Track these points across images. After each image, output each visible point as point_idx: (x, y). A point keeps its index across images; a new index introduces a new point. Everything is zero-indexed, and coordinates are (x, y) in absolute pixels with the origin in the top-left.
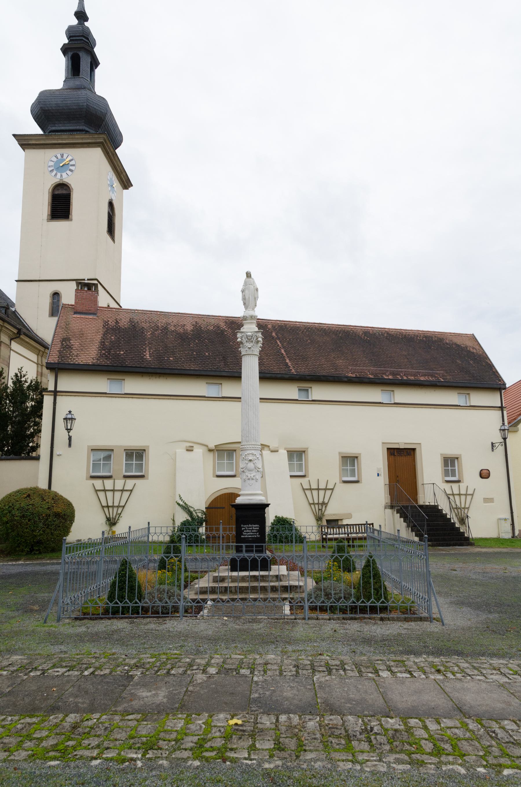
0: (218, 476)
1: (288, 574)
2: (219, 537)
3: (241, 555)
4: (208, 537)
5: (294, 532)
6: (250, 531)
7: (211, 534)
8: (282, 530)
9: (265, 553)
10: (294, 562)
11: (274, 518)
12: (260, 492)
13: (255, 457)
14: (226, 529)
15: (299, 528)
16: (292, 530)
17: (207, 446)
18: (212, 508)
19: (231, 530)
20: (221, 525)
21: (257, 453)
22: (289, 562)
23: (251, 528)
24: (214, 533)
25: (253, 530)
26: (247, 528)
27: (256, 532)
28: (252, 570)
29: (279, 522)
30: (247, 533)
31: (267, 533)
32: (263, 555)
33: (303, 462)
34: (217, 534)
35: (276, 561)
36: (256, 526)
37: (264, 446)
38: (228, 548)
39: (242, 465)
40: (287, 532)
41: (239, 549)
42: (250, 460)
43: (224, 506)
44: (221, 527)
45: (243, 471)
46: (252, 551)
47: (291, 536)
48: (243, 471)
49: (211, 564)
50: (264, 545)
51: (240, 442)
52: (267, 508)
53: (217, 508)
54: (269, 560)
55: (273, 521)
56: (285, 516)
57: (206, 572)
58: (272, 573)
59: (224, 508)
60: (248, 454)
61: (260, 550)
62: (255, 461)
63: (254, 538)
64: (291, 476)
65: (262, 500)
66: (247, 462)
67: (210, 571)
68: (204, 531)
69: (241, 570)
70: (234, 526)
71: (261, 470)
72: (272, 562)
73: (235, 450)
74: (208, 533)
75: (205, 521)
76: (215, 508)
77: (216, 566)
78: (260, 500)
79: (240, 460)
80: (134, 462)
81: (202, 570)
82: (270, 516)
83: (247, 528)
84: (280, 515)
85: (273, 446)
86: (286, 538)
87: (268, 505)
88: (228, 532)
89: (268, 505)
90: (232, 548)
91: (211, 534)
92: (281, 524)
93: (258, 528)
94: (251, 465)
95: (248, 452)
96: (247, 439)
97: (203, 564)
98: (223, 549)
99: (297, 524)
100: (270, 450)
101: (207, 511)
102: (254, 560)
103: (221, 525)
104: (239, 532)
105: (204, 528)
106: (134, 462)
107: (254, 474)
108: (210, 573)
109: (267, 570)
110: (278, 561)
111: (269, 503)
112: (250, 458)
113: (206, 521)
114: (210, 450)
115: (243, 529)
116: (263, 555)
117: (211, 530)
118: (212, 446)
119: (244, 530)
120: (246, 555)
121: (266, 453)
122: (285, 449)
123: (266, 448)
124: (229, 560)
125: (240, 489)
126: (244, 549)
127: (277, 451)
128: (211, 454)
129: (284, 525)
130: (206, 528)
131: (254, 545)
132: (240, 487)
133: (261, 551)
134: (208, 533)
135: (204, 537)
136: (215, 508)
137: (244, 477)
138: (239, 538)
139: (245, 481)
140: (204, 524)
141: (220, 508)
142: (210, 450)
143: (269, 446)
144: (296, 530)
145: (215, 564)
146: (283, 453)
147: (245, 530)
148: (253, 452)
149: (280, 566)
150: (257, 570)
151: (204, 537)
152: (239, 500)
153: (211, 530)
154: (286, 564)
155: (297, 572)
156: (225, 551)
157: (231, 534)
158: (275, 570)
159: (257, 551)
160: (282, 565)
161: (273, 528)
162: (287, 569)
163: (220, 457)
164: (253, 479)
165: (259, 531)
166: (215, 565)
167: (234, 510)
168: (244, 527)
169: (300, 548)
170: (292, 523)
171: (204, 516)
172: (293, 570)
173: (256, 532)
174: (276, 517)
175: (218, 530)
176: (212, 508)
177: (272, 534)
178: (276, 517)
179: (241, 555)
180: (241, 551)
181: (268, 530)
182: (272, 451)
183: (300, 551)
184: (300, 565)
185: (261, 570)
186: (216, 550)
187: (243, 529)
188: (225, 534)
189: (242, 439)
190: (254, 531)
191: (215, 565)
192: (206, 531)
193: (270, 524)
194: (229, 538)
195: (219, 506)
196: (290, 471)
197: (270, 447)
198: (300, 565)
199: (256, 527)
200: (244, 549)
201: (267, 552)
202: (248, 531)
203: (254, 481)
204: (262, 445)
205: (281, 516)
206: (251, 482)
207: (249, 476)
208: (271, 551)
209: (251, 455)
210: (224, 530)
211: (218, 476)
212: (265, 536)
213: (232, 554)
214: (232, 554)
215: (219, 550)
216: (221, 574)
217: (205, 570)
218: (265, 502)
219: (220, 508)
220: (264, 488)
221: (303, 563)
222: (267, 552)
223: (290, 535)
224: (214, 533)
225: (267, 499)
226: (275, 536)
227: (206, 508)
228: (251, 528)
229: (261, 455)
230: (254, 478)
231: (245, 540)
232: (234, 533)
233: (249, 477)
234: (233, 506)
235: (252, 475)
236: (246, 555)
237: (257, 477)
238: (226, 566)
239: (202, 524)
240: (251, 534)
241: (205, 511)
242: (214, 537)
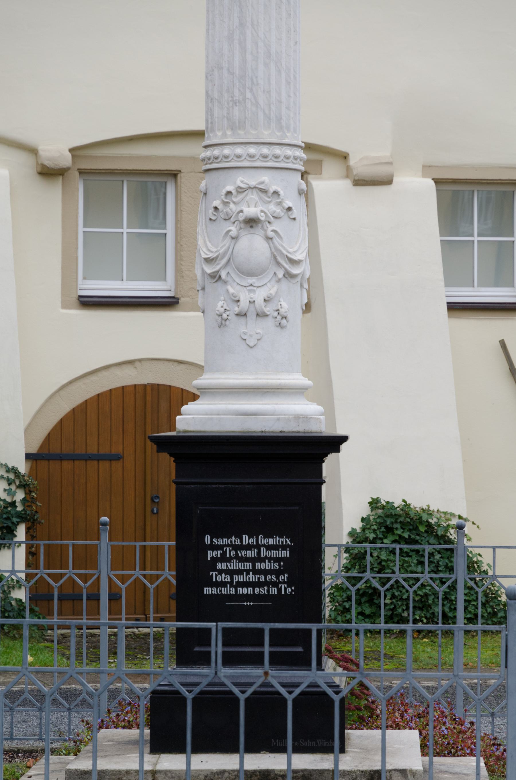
0: (88, 303)
1: (428, 770)
2: (94, 598)
3: (202, 676)
4: (40, 597)
5: (461, 575)
6: (247, 563)
7: (56, 578)
8: (403, 568)
9: (320, 667)
10: (459, 713)
11: (366, 511)
12: (297, 379)
13: (272, 207)
14: (128, 555)
15: (486, 558)
16: (451, 570)
17: (33, 151)
18: (61, 458)
19: (151, 559)
20: (105, 537)
21: (287, 186)
22: (433, 714)
23: (251, 554)
24: (70, 572)
25: (262, 560)
26: (230, 552)
27: (278, 573)
28: (253, 748)
29: (389, 530)
30: (231, 573)
31: (327, 583)
32: (304, 678)
33: (170, 230)
34: (85, 578)
35: (371, 708)
36: (277, 540)
37: (318, 156)
38: (138, 647)
39: (208, 243)
40: (426, 577)
41: (189, 649)
42: (251, 222)
43: (116, 449)
44: (104, 546)
45: (216, 277)
46: (256, 660)
47: (446, 597)
48: (216, 277)
49: (57, 717)
50: (314, 627)
51: (199, 134)
52: (331, 457)
53: (87, 458)
54: (337, 699)
55: (358, 526)
56: (417, 503)
57: (32, 754)
58: (348, 762)
59: (118, 458)
60: (240, 190)
61: (296, 653)
62: (276, 226)
63: (268, 597)
64: (454, 308)
65: (306, 418)
66: (234, 230)
67: (53, 751)
68: (21, 563)
69: (200, 748)
70: (169, 545)
71: (304, 269)
72: (352, 715)
73: (174, 175)
74: (42, 572)
75: (22, 518)
76: (73, 458)
77: (82, 729)
78: (298, 418)
79: (202, 220)
80: (125, 230)
81: (15, 745)
82: (348, 499)
83: (230, 552)
84: (394, 496)
85: (364, 156)
86: (423, 604)
87: (335, 443)
88: (138, 573)
89: (335, 443)
90: (159, 652)
91: (56, 578)
92: (400, 540)
93: (286, 554)
94: (253, 247)
95: (241, 179)
96: (236, 112)
97: (18, 717)
98: (113, 652)
99: (477, 540)
100: (348, 173)
101: (33, 472)
102: (266, 703)
103: (105, 537)
104: (193, 569)
105: (21, 553)
106: (125, 230)
107: (271, 289)
108: (53, 759)
109: (328, 750)
110: (382, 708)
111: (340, 432)
112: (251, 211)
113: (30, 520)
114: (48, 173)
115: (210, 554)
116: (304, 678)
117: (56, 558)
118: (56, 149)
119: (215, 560)
120: (228, 676)
121: (329, 187)
122: (427, 169)
123: (330, 166)
124: (145, 702)
125: (200, 368)
126: (217, 648)
127: (387, 181)
128: (55, 191)
129: (410, 541)
130: (32, 554)
131: (267, 626)
132: (199, 359)
133: (302, 661)
134: (42, 572)
135: (20, 594)
136: (73, 458)
137: (220, 306)
138: (191, 595)
139: (222, 322)
140: (21, 533)
141: (99, 458)
142: (48, 173)
143: (345, 157)
144: (472, 566)
145: (76, 721)
146: (417, 191)
147: (224, 558)
148: (265, 178)
149: (389, 733)
150: (279, 749)
151: (20, 594)
152: (194, 419)
153: (56, 558)
154: (419, 721)
155: (471, 761)
156: (124, 666)
157: (152, 579)
158: (366, 750)
159: (279, 661)
160: (398, 727)
161: (357, 559)
162: (424, 747)
163: (99, 209)
164: (261, 315)
165: (287, 566)
166: (75, 722)
167: (167, 463)
168: (218, 546)
169: (487, 655)
170: (452, 534)
171: (20, 495)
172: (451, 750)
173: (278, 573)
174: (374, 503)
175: (87, 559)
176: (61, 458)
177: (357, 580)
178: (374, 503)
179: (202, 676)
180: (204, 660)
181: (333, 563)
182: (360, 182)
183: (488, 666)
184: (485, 728)
185: (298, 749)
186: (79, 655)
187: (210, 554)
188: (123, 579)
189: (209, 112)
190: (268, 565)
191: (75, 722)
192: (28, 565)
193: (345, 540)
194: (145, 602)
195: (93, 450)
196: (448, 284)
197: (352, 161)
198: (485, 728)
199: (274, 547)
200: (217, 648)
201: (329, 664)
202: (235, 565)
203: (269, 323)
204: (309, 147)
205: (398, 503)
206: (254, 328)
207: (244, 297)
208: (346, 662)
209: (254, 196)
210: (121, 559)
211: (88, 303)
212: (320, 592)
213: (165, 672)
214: (165, 672)
215: (96, 658)
216: (103, 764)
217: (27, 745)
218: (322, 428)
219: (99, 458)
220: (318, 360)
221: (499, 721)
222: (329, 664)
223: (441, 590)
224: (70, 572)
225: (330, 412)
226: (370, 596)
227: (28, 456)
228: (251, 554)
229: (306, 195)
230: (268, 310)
231: (222, 608)
232: (169, 574)
233: (244, 304)
234: (164, 444)
235: (259, 296)
236: (228, 676)
237: (285, 306)
238: (129, 727)
239: (11, 532)
240: (252, 578)
241: (23, 468)
242: (71, 599)
